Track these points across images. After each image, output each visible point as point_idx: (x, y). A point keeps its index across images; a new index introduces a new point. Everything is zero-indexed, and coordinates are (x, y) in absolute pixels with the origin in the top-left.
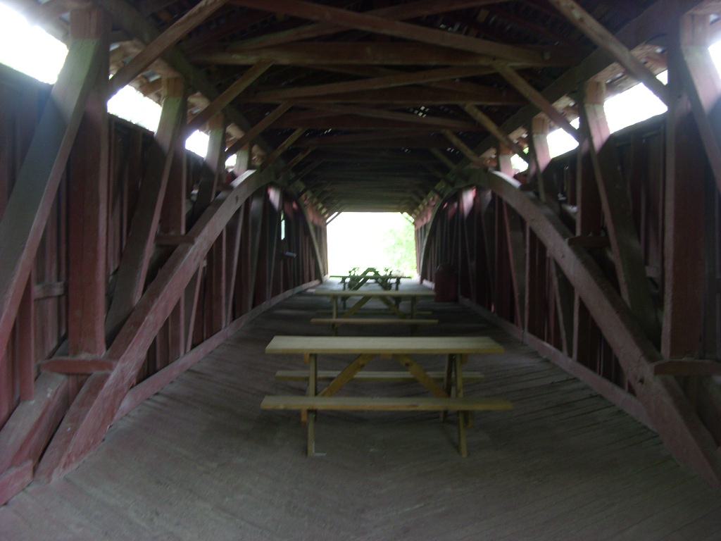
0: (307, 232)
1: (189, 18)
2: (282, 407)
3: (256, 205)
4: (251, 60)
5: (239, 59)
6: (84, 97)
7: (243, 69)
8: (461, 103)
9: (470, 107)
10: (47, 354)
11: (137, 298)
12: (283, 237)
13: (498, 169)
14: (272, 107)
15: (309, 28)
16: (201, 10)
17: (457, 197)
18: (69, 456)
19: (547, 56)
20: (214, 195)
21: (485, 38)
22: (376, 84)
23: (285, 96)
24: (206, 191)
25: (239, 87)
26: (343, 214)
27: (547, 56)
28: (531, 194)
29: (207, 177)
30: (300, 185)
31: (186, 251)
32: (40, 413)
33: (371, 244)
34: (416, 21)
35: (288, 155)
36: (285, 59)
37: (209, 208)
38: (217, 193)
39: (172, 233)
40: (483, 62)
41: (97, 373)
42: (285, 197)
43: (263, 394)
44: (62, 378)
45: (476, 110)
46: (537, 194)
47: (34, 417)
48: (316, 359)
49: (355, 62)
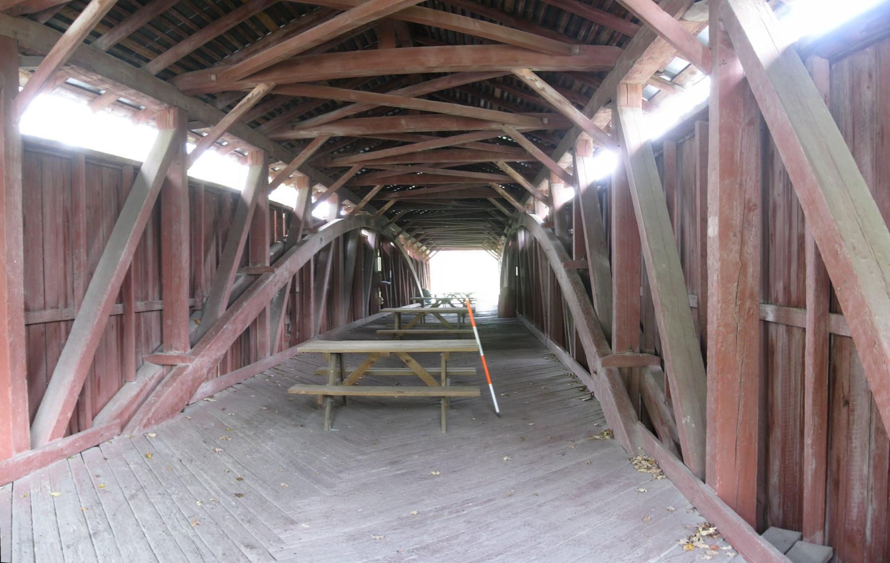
0: (406, 266)
1: (241, 106)
2: (303, 392)
3: (351, 245)
4: (314, 134)
5: (304, 134)
6: (165, 166)
7: (307, 142)
8: (494, 161)
9: (501, 163)
10: (150, 350)
11: (221, 311)
12: (379, 269)
13: (534, 212)
14: (346, 169)
15: (349, 107)
16: (249, 100)
17: (514, 238)
18: (148, 420)
19: (546, 121)
20: (300, 237)
21: (505, 111)
22: (418, 147)
23: (356, 161)
24: (294, 233)
25: (306, 154)
26: (440, 252)
27: (546, 121)
28: (550, 230)
29: (295, 226)
30: (393, 229)
31: (267, 278)
32: (138, 390)
33: (465, 277)
34: (431, 97)
35: (376, 203)
36: (339, 131)
37: (294, 247)
38: (303, 236)
39: (259, 265)
40: (494, 126)
41: (181, 364)
42: (382, 239)
43: (293, 384)
44: (158, 367)
45: (506, 165)
46: (553, 230)
47: (134, 393)
48: (591, 399)
49: (393, 131)
